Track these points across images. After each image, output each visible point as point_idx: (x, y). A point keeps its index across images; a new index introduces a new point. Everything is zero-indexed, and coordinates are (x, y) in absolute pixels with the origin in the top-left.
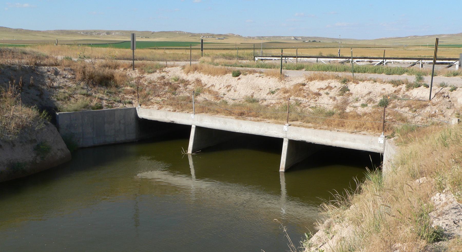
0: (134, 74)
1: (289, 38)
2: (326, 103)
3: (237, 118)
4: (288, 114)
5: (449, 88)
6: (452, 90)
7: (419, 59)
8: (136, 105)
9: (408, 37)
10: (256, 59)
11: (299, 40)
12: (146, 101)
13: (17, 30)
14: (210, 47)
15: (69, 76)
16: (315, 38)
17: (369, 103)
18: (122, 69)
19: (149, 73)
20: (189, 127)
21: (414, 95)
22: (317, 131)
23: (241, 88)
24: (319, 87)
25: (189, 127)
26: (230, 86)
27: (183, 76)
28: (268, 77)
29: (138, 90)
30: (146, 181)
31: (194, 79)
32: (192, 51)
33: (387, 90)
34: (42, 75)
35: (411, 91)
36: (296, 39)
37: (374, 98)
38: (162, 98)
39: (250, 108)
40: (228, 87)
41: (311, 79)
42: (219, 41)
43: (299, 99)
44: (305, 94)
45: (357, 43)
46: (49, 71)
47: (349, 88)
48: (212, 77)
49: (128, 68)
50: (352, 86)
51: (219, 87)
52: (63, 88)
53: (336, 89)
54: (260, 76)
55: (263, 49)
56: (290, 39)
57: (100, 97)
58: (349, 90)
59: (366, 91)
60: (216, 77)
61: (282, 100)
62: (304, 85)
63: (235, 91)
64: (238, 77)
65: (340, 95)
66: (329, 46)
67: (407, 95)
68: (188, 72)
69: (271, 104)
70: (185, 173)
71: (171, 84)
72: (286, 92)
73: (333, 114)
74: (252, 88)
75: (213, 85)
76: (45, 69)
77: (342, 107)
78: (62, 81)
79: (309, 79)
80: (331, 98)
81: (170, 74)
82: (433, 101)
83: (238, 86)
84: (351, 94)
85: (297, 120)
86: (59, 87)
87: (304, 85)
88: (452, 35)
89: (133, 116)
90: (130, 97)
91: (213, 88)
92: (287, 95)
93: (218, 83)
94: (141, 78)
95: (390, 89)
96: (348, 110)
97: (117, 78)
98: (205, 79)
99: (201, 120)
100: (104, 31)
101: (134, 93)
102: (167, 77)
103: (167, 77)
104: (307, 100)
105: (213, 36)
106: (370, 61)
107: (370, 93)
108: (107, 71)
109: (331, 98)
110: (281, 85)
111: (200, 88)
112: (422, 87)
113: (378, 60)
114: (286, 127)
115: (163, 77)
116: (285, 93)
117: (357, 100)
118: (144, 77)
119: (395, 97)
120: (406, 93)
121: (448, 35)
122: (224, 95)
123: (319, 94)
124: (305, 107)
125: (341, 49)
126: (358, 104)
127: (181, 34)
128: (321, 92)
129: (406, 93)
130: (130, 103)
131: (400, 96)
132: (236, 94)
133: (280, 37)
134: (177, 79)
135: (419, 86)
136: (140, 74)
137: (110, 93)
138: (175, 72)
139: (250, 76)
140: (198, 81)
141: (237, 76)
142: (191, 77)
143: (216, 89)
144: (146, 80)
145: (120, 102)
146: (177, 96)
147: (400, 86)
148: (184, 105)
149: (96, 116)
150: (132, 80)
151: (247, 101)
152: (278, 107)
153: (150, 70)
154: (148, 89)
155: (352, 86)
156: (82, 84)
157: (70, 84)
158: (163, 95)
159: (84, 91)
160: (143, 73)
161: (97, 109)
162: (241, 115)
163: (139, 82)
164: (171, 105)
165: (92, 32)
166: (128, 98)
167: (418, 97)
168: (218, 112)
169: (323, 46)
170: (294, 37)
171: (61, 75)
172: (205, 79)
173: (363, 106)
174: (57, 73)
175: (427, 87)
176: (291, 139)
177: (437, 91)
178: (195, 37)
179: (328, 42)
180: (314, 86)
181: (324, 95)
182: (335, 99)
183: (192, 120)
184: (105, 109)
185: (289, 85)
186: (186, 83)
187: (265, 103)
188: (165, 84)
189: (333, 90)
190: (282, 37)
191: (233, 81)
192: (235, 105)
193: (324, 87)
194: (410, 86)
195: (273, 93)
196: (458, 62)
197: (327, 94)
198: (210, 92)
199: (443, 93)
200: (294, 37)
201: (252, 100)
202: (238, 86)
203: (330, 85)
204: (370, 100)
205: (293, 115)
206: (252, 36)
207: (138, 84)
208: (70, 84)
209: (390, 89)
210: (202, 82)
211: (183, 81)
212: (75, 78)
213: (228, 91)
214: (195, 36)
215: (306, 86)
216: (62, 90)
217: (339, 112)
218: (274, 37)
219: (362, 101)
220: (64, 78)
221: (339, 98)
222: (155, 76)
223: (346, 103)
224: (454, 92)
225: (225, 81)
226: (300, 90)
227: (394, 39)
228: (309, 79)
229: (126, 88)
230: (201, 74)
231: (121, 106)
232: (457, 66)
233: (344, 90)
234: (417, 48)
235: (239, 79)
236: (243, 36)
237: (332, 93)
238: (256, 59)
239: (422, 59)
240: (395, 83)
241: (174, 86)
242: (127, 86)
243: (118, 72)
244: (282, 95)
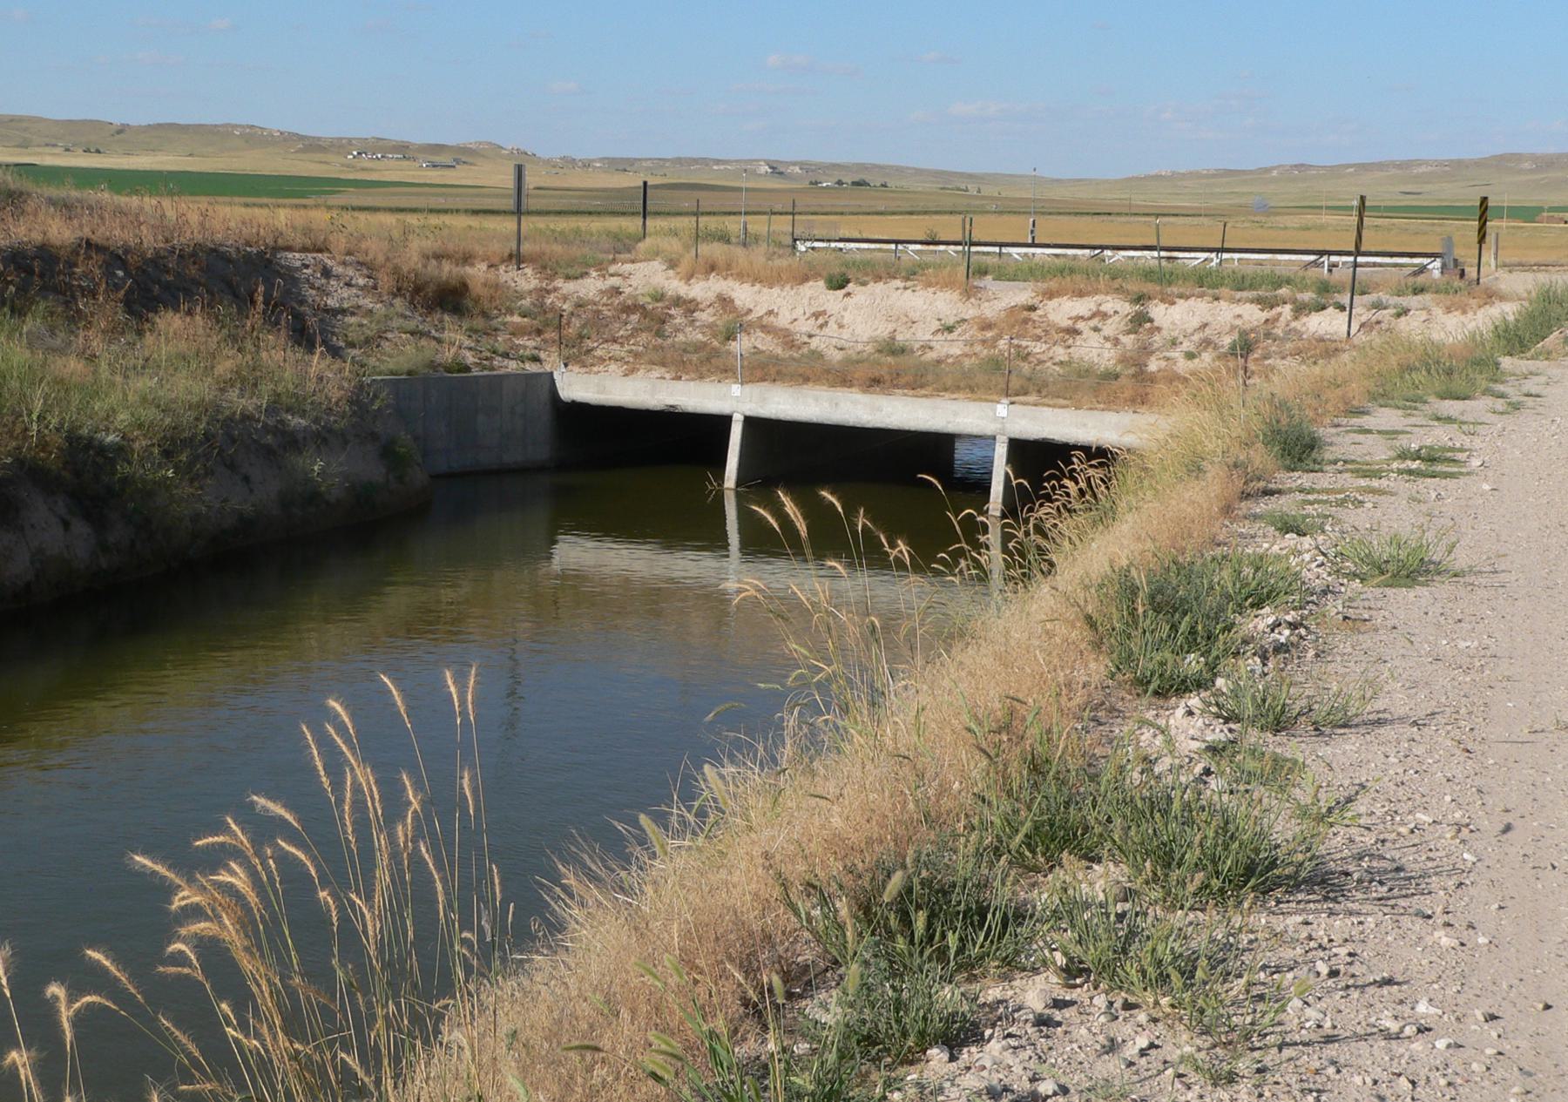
0: (526, 280)
2: (1095, 351)
3: (864, 392)
4: (1002, 376)
5: (1392, 311)
6: (1399, 315)
7: (1321, 253)
8: (552, 362)
9: (1268, 170)
10: (801, 247)
11: (790, 177)
12: (578, 354)
14: (403, 203)
15: (361, 282)
16: (864, 167)
17: (1205, 349)
18: (483, 266)
19: (568, 278)
20: (726, 421)
21: (1312, 330)
22: (1083, 415)
23: (860, 317)
24: (1074, 314)
25: (726, 421)
26: (824, 312)
27: (674, 285)
28: (931, 290)
29: (546, 321)
30: (574, 580)
31: (711, 296)
33: (1246, 317)
34: (290, 276)
35: (1305, 319)
36: (776, 170)
37: (1214, 338)
38: (627, 348)
39: (892, 367)
40: (816, 315)
41: (1050, 295)
42: (435, 176)
43: (1024, 343)
44: (1038, 331)
46: (307, 267)
47: (1152, 315)
48: (765, 290)
49: (503, 261)
50: (1158, 311)
51: (789, 318)
52: (353, 314)
53: (1116, 318)
54: (905, 288)
55: (746, 213)
56: (754, 174)
57: (455, 343)
58: (1151, 321)
59: (1195, 323)
60: (776, 291)
61: (978, 348)
62: (1033, 308)
63: (841, 326)
64: (843, 291)
65: (1129, 332)
66: (932, 207)
67: (1295, 330)
68: (689, 277)
69: (948, 356)
71: (643, 307)
72: (986, 326)
73: (1117, 377)
74: (889, 319)
75: (770, 312)
76: (294, 259)
77: (1136, 363)
78: (346, 292)
79: (1044, 294)
80: (1106, 339)
81: (634, 281)
82: (1356, 341)
83: (846, 314)
84: (1159, 329)
85: (1026, 394)
86: (343, 311)
87: (1033, 308)
88: (1459, 164)
89: (545, 396)
90: (531, 344)
91: (772, 318)
92: (989, 334)
93: (791, 306)
94: (548, 292)
95: (1253, 315)
96: (1153, 365)
97: (476, 288)
98: (744, 295)
101: (539, 332)
102: (628, 290)
103: (628, 290)
104: (1044, 347)
105: (404, 150)
106: (1169, 258)
107: (1205, 325)
108: (448, 270)
109: (1106, 339)
110: (970, 311)
111: (735, 324)
112: (1331, 310)
113: (1193, 255)
114: (1002, 409)
115: (616, 291)
116: (983, 329)
117: (1174, 343)
118: (556, 289)
119: (1268, 335)
120: (1293, 324)
121: (1440, 164)
122: (810, 336)
123: (1073, 332)
124: (1041, 362)
125: (1040, 220)
126: (1176, 354)
127: (254, 137)
128: (1080, 325)
129: (1293, 324)
130: (536, 359)
131: (1279, 332)
132: (846, 334)
133: (705, 162)
134: (659, 297)
135: (1324, 308)
136: (541, 281)
137: (476, 331)
138: (645, 276)
139: (878, 288)
140: (725, 302)
141: (841, 287)
142: (703, 290)
143: (783, 321)
144: (565, 299)
145: (506, 355)
146: (670, 341)
147: (1279, 309)
148: (707, 361)
149: (453, 392)
150: (522, 297)
151: (880, 351)
152: (967, 363)
153: (571, 272)
154: (576, 322)
155: (1158, 311)
156: (398, 302)
157: (367, 302)
158: (628, 338)
159: (411, 325)
160: (551, 278)
161: (459, 371)
162: (874, 383)
163: (542, 305)
164: (663, 365)
166: (525, 348)
167: (1321, 332)
168: (807, 380)
169: (906, 207)
170: (768, 163)
171: (338, 277)
172: (744, 295)
173: (1190, 356)
174: (327, 273)
175: (1342, 308)
176: (1017, 436)
177: (1364, 319)
178: (319, 156)
180: (1062, 310)
181: (1087, 333)
182: (1116, 342)
183: (734, 400)
184: (476, 372)
185: (991, 310)
186: (690, 307)
187: (931, 356)
188: (628, 309)
189: (1110, 321)
190: (718, 162)
191: (832, 301)
192: (848, 361)
193: (1087, 314)
194: (1301, 310)
195: (950, 329)
196: (1438, 263)
197: (1096, 329)
198: (766, 329)
199: (1378, 322)
200: (768, 163)
201: (892, 348)
202: (846, 314)
203: (1102, 308)
204: (1207, 343)
205: (1015, 383)
207: (542, 308)
208: (367, 302)
209: (1253, 315)
210: (738, 303)
211: (678, 301)
212: (375, 287)
213: (821, 327)
215: (1039, 312)
216: (352, 320)
217: (1132, 371)
218: (679, 161)
219: (1187, 346)
220: (348, 285)
221: (1128, 340)
222: (591, 287)
223: (1146, 350)
224: (1403, 319)
225: (806, 301)
226: (1026, 321)
227: (1207, 176)
228: (1044, 294)
229: (508, 319)
230: (731, 283)
231: (512, 366)
232: (1437, 274)
233: (1140, 321)
234: (1310, 219)
235: (849, 294)
237: (1109, 328)
238: (801, 247)
239: (1330, 253)
240: (1267, 303)
241: (654, 316)
242: (512, 314)
243: (477, 273)
244: (973, 332)
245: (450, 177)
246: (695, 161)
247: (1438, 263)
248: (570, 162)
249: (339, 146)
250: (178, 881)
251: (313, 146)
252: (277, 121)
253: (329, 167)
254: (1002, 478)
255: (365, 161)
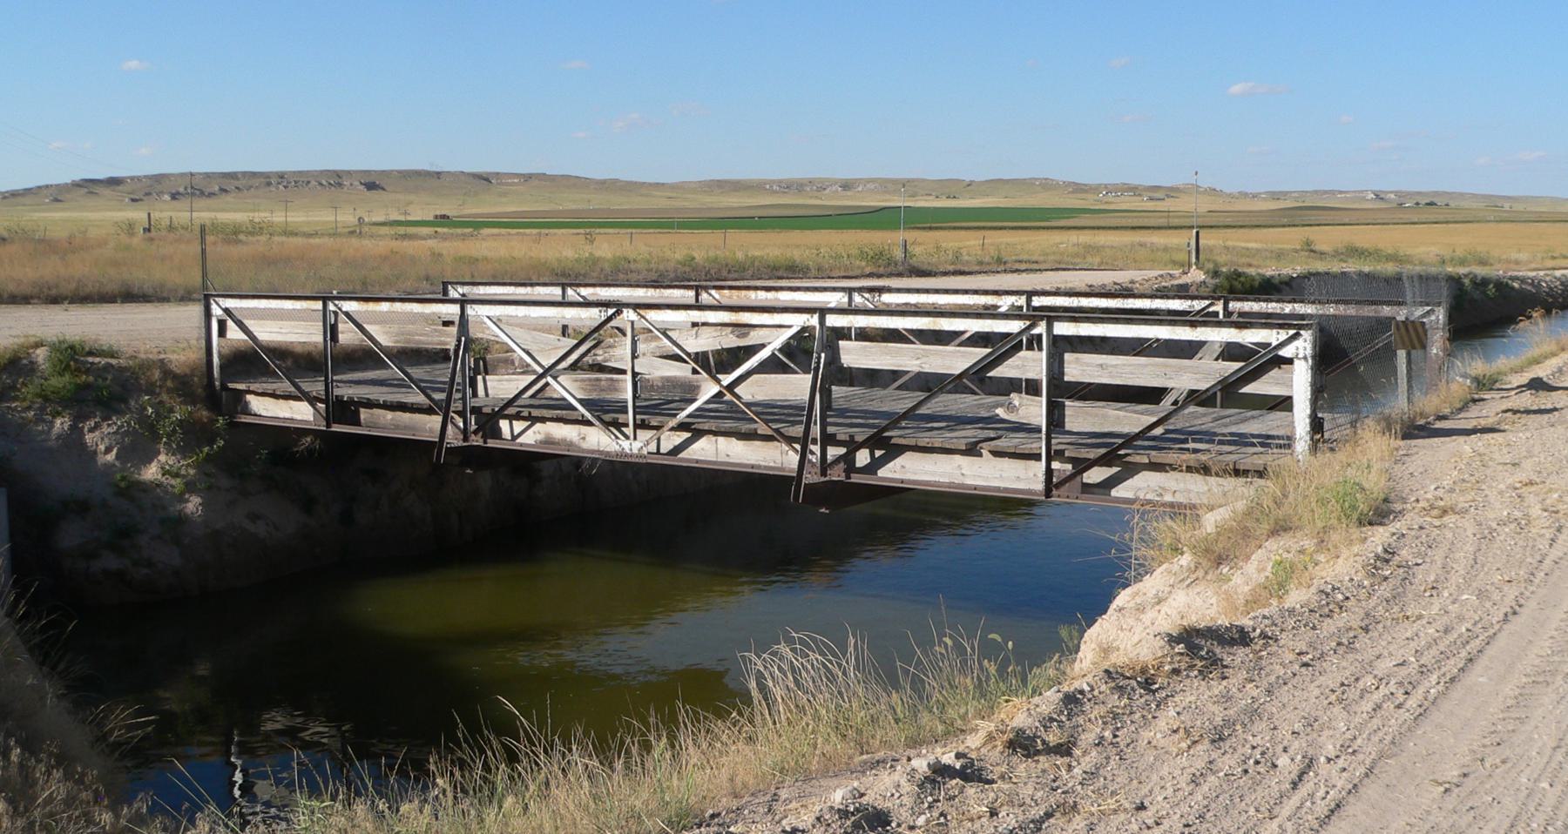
1: (1359, 195)
13: (603, 182)
14: (1124, 222)
16: (1437, 194)
32: (560, 299)
36: (1379, 196)
42: (1150, 206)
45: (1560, 209)
56: (1364, 199)
70: (263, 375)
99: (1305, 358)
100: (834, 182)
105: (1135, 190)
127: (1047, 185)
133: (1332, 192)
165: (802, 185)
179: (1474, 205)
206: (1251, 189)
214: (1086, 191)
236: (1227, 190)
245: (1160, 206)
246: (1326, 192)
247: (1303, 347)
248: (1244, 195)
249: (1095, 189)
250: (336, 428)
251: (1079, 189)
252: (1060, 175)
253: (1089, 202)
254: (962, 329)
255: (1110, 197)
